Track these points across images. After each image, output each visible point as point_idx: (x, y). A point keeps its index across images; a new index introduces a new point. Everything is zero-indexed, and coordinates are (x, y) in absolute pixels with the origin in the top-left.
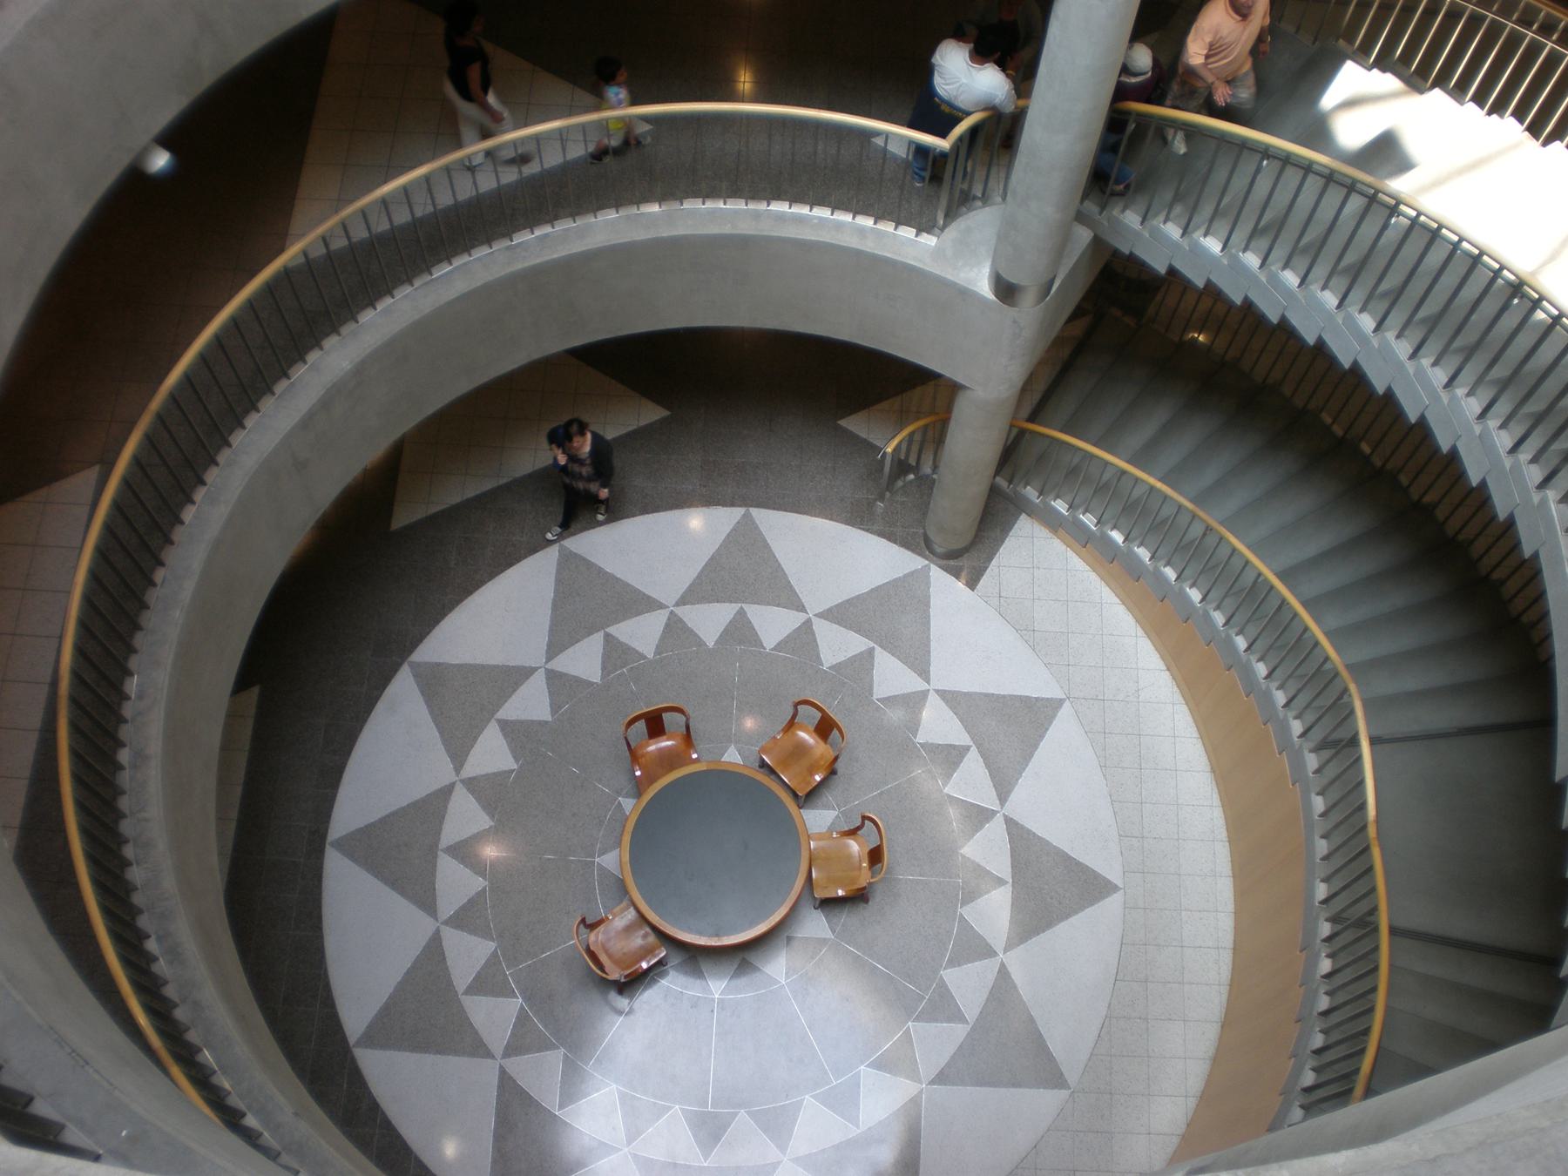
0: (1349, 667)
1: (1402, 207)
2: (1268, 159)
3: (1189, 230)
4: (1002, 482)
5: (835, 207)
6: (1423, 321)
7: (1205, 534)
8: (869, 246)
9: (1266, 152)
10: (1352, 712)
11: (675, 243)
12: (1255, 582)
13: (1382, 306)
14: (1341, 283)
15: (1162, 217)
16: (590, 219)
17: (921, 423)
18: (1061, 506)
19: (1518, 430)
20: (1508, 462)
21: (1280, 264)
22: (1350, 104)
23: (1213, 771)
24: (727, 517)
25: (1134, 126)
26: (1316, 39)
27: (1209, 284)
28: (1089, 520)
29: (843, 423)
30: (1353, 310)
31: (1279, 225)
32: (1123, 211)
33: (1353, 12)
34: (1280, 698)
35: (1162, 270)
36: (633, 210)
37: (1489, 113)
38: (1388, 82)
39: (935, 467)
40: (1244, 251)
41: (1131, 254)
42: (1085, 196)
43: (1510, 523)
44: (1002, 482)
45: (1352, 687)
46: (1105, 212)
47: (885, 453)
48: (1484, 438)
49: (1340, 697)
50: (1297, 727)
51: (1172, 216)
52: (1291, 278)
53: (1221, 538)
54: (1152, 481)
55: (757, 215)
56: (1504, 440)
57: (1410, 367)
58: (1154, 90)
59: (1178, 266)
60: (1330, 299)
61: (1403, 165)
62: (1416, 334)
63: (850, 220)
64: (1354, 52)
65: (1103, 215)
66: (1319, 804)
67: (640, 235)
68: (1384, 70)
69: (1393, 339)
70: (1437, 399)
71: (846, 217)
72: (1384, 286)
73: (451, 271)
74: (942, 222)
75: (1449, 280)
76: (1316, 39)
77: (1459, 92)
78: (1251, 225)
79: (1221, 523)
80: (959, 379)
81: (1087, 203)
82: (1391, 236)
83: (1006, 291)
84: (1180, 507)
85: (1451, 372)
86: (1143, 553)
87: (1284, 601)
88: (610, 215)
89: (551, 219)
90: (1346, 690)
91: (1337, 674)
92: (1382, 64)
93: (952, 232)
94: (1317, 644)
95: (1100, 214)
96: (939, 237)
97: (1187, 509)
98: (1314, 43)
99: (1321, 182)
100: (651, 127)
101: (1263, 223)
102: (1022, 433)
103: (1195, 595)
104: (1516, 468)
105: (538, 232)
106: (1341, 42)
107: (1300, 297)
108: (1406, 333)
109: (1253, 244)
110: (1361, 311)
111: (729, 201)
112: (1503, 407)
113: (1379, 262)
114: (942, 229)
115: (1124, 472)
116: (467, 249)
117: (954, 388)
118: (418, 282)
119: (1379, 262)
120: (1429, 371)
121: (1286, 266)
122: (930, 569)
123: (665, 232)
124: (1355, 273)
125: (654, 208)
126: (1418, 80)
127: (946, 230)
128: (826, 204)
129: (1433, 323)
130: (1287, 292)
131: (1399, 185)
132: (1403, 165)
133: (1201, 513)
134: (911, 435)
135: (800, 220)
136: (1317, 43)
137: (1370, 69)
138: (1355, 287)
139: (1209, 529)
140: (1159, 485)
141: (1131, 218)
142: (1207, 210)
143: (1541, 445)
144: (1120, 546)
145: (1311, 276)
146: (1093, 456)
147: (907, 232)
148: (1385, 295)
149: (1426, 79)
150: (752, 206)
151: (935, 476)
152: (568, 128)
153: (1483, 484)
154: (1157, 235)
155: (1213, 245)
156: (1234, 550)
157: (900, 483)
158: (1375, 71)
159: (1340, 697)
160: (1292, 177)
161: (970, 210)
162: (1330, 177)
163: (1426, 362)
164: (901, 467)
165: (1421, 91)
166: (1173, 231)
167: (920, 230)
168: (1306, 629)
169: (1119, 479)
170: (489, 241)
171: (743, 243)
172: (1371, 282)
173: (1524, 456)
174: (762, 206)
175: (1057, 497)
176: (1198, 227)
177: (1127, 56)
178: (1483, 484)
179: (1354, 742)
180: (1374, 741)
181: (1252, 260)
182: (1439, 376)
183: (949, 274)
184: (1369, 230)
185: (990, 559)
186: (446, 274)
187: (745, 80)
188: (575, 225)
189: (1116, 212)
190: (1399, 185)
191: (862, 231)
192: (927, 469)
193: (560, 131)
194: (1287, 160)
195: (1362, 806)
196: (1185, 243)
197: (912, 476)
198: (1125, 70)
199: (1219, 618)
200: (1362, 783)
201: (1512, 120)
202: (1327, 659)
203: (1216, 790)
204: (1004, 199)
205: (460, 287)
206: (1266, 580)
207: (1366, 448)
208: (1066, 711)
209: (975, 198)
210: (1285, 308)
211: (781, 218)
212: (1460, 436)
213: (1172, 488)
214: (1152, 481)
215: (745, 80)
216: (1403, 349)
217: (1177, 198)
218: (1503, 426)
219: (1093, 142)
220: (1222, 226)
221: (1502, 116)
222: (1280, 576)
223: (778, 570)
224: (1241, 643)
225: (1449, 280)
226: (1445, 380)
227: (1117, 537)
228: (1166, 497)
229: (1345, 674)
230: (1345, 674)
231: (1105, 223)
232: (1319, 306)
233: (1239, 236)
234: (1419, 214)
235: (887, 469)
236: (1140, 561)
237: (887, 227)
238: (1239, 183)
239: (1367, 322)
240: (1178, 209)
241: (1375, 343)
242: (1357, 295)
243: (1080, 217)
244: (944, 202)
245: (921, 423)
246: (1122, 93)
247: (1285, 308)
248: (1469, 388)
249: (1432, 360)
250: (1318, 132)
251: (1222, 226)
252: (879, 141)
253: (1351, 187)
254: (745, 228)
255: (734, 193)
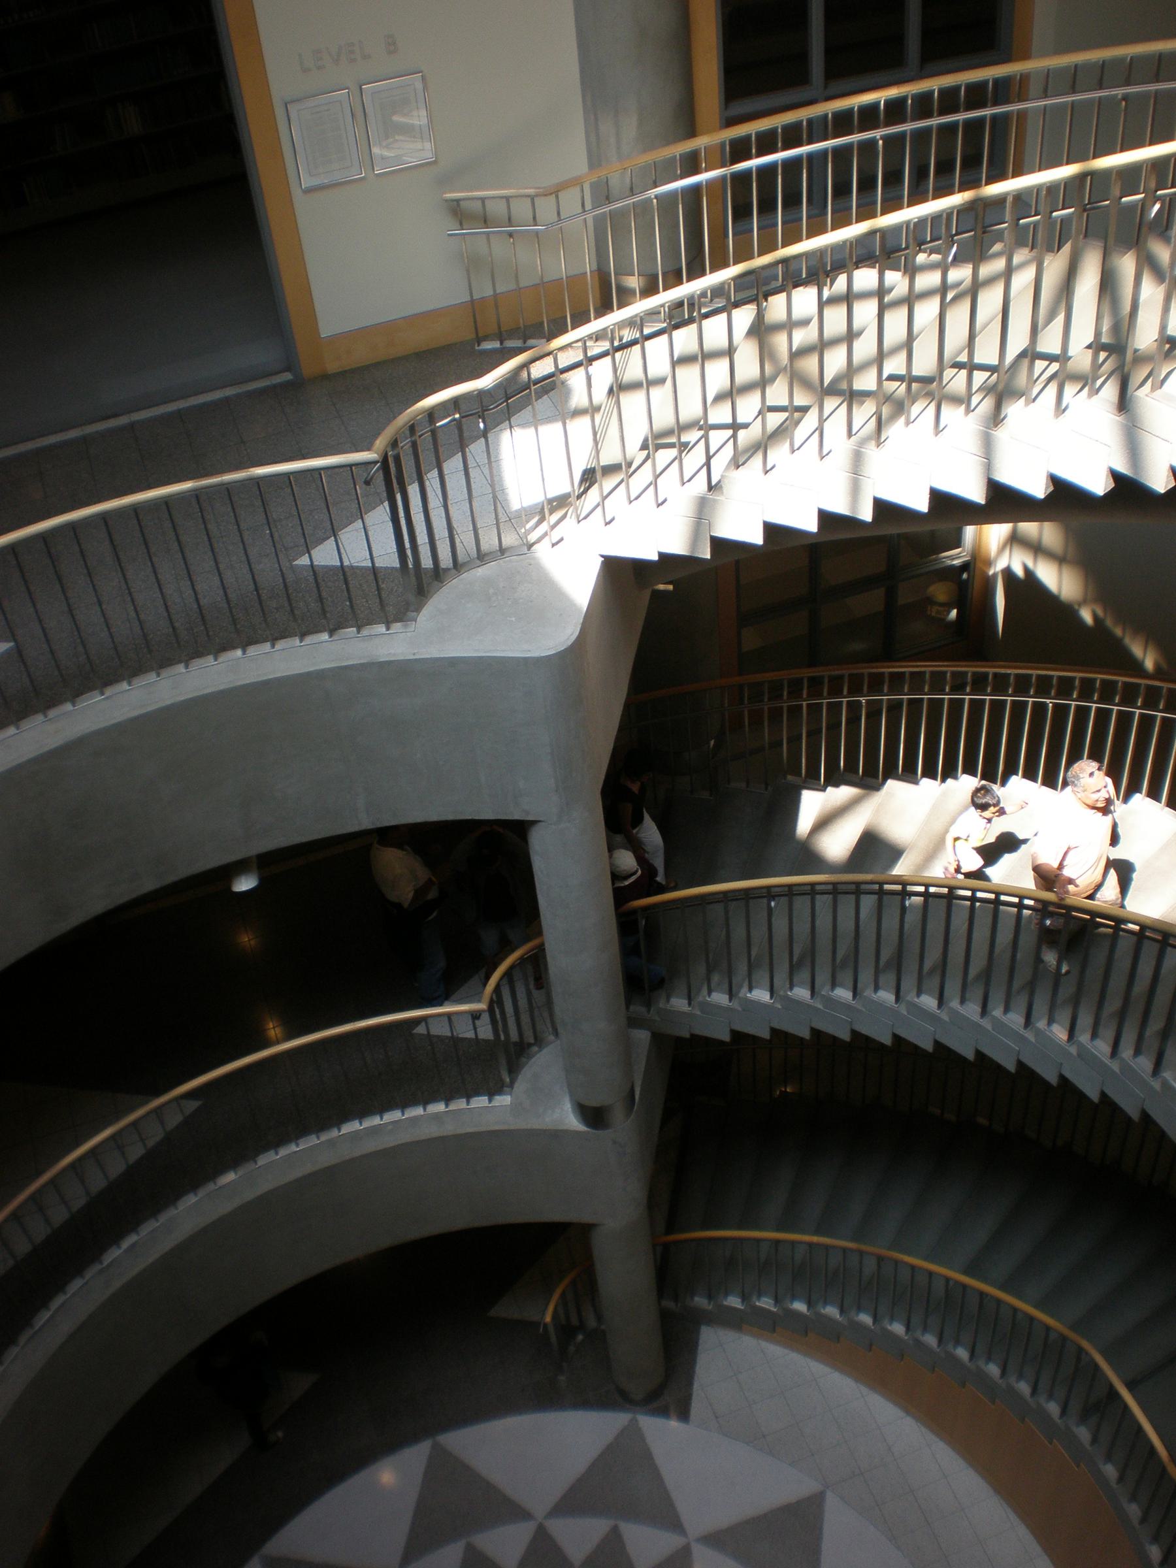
0: (1073, 1328)
1: (910, 888)
2: (774, 900)
3: (734, 992)
4: (669, 1304)
5: (404, 1106)
6: (978, 978)
7: (879, 1266)
8: (449, 1129)
9: (769, 893)
10: (1096, 1367)
11: (264, 1200)
12: (947, 1290)
13: (935, 982)
14: (889, 978)
15: (705, 991)
16: (171, 1213)
17: (566, 1281)
18: (734, 1302)
19: (1108, 1033)
20: (1115, 1066)
21: (828, 987)
22: (823, 823)
23: (998, 1491)
24: (416, 1456)
25: (644, 923)
26: (767, 785)
27: (774, 1031)
28: (766, 1303)
29: (494, 1312)
30: (911, 997)
31: (811, 953)
32: (668, 1000)
33: (788, 749)
34: (1024, 1388)
35: (726, 1037)
36: (211, 1187)
37: (943, 780)
38: (844, 793)
39: (599, 1318)
40: (791, 989)
41: (692, 1035)
42: (628, 1003)
43: (1145, 1116)
44: (669, 1304)
45: (1085, 1344)
46: (652, 1009)
47: (545, 1325)
48: (1083, 1054)
49: (1079, 1359)
50: (1053, 1408)
51: (713, 985)
52: (843, 994)
53: (896, 1262)
54: (806, 1238)
55: (331, 1143)
56: (1102, 1047)
57: (986, 1023)
58: (648, 884)
59: (738, 1027)
60: (886, 996)
61: (895, 853)
62: (977, 993)
63: (422, 1113)
64: (804, 782)
65: (651, 1012)
66: (1110, 1471)
67: (225, 1207)
68: (836, 785)
69: (959, 1006)
70: (1024, 1039)
71: (418, 1111)
72: (928, 964)
73: (52, 1317)
74: (508, 1080)
75: (981, 934)
76: (767, 785)
77: (909, 775)
78: (786, 965)
79: (889, 1249)
80: (586, 1218)
81: (632, 1008)
82: (911, 919)
83: (594, 1116)
84: (845, 1250)
85: (1024, 1010)
86: (832, 1311)
87: (982, 1294)
88: (191, 1200)
89: (134, 1227)
90: (1080, 1350)
91: (1064, 1339)
92: (834, 779)
93: (521, 1084)
94: (1031, 1319)
95: (649, 1011)
96: (511, 1095)
97: (851, 1250)
98: (766, 789)
99: (828, 898)
100: (200, 1103)
101: (795, 959)
102: (666, 1246)
103: (898, 1328)
104: (1125, 1067)
105: (126, 1244)
106: (789, 777)
107: (860, 1007)
108: (967, 996)
109: (795, 980)
110: (919, 995)
111: (301, 1141)
112: (1085, 1020)
113: (913, 946)
114: (511, 1085)
115: (777, 1242)
116: (60, 1288)
117: (586, 1230)
118: (23, 1339)
119: (913, 946)
120: (1004, 1019)
121: (834, 985)
122: (636, 1421)
123: (249, 1195)
124: (898, 964)
125: (230, 1177)
126: (870, 780)
127: (516, 1085)
128: (830, 138)
129: (987, 975)
130: (847, 1007)
131: (901, 869)
132: (895, 853)
133: (864, 1247)
134: (563, 1295)
135: (374, 1130)
136: (769, 788)
137: (823, 789)
138: (903, 978)
139: (880, 1259)
140: (815, 1239)
141: (679, 1003)
142: (742, 968)
143: (1136, 1037)
144: (807, 1315)
145: (859, 985)
146: (741, 1240)
147: (480, 1102)
148: (932, 971)
149: (876, 777)
150: (325, 1137)
151: (603, 1327)
152: (120, 1132)
153: (1103, 1095)
154: (707, 1008)
155: (761, 995)
156: (913, 1268)
157: (572, 1348)
158: (829, 789)
159: (1079, 1359)
160: (802, 905)
161: (530, 1057)
162: (835, 890)
163: (997, 1012)
164: (567, 1331)
165: (877, 788)
166: (720, 998)
167: (491, 1095)
168: (1015, 1310)
169: (777, 1250)
170: (79, 1271)
171: (330, 1174)
172: (915, 967)
173: (1127, 1052)
174: (334, 1133)
175: (726, 1295)
176: (741, 987)
177: (612, 865)
178: (1103, 1095)
179: (1113, 1394)
180: (1131, 1386)
181: (801, 993)
182: (1015, 1019)
183: (535, 1124)
184: (890, 922)
185: (690, 1384)
186: (48, 1321)
187: (273, 1029)
188: (159, 1224)
189: (662, 1004)
190: (901, 869)
191: (437, 1117)
192: (592, 1323)
193: (112, 1137)
194: (790, 891)
195: (1152, 1450)
196: (735, 1004)
197: (580, 1337)
198: (616, 876)
199: (930, 1340)
200: (1140, 1429)
201: (965, 776)
202: (1048, 1329)
203: (1009, 1510)
204: (556, 1034)
205: (66, 1327)
206: (957, 1282)
207: (982, 1121)
208: (832, 1502)
209: (530, 1045)
210: (851, 1023)
211: (355, 1136)
212: (1061, 1064)
213: (828, 1236)
214: (806, 1238)
215: (273, 1029)
216: (971, 1010)
217: (710, 971)
218: (1094, 1035)
219: (615, 948)
220: (762, 975)
221: (956, 778)
222: (967, 1272)
223: (489, 1488)
224: (962, 1353)
225: (981, 934)
226: (1022, 1021)
227: (800, 1306)
228: (827, 1247)
229: (1071, 1335)
230: (1071, 1335)
231: (657, 1018)
232: (881, 1005)
233: (781, 978)
234: (927, 886)
235: (553, 1339)
236: (830, 1319)
237: (460, 1104)
238: (759, 934)
239: (928, 1002)
240: (716, 978)
241: (945, 1017)
242: (909, 983)
243: (633, 1022)
244: (503, 1061)
245: (566, 1281)
246: (621, 896)
247: (851, 1023)
248: (1047, 1017)
249: (1002, 1009)
250: (808, 857)
251: (762, 975)
252: (421, 1030)
253: (857, 890)
254: (327, 1159)
255: (303, 1131)
